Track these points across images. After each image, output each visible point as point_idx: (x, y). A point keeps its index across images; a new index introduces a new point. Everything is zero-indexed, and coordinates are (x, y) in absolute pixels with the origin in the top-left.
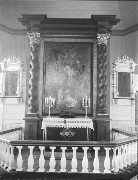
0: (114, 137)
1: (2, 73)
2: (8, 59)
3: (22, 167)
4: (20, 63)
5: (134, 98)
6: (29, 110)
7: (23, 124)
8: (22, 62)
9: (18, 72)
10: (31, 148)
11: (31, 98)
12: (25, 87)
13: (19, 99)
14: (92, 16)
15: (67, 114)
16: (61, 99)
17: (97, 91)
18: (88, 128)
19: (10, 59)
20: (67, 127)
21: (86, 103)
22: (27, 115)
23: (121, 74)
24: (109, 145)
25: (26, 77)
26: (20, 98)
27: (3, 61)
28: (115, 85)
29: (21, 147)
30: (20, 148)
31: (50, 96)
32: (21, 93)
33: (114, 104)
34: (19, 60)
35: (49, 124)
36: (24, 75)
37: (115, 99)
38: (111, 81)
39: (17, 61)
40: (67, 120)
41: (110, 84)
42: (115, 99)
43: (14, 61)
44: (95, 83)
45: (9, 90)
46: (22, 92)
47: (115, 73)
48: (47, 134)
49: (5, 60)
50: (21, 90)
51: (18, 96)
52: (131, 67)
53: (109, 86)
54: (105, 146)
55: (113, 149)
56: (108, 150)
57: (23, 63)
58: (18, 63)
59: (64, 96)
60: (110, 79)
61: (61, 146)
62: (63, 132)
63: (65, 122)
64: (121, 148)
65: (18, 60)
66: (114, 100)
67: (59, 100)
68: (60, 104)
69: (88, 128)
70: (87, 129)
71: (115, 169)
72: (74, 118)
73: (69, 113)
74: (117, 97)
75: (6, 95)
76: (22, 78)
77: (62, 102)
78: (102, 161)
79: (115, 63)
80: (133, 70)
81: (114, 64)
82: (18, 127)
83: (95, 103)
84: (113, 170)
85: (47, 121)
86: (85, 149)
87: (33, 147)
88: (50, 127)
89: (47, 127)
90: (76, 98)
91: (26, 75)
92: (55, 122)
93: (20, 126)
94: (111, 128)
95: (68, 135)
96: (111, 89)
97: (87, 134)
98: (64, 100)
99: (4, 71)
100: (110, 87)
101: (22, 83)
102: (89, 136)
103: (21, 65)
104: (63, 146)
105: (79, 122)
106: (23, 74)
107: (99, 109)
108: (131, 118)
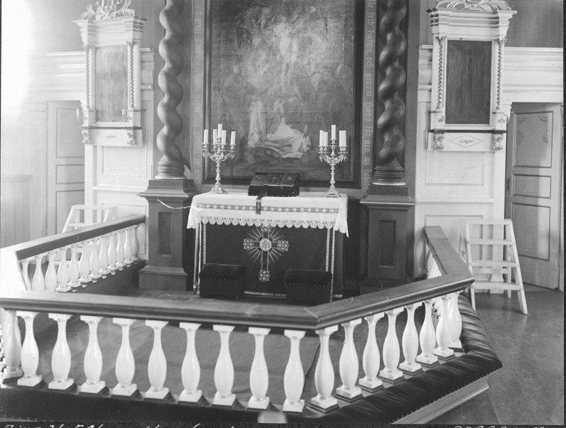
1: (84, 53)
2: (100, 10)
5: (503, 127)
6: (160, 169)
7: (142, 208)
8: (136, 17)
11: (165, 130)
13: (131, 132)
15: (270, 181)
16: (260, 133)
17: (375, 104)
18: (332, 230)
19: (104, 9)
20: (266, 225)
23: (457, 47)
25: (153, 64)
26: (135, 128)
27: (85, 14)
28: (435, 87)
29: (65, 318)
30: (62, 319)
31: (334, 127)
33: (430, 148)
34: (130, 11)
35: (247, 217)
36: (145, 57)
37: (432, 131)
38: (423, 73)
39: (122, 15)
40: (267, 201)
41: (420, 81)
42: (432, 131)
43: (115, 13)
44: (368, 78)
45: (106, 105)
46: (143, 111)
47: (436, 46)
48: (205, 243)
49: (90, 11)
50: (137, 105)
51: (131, 124)
52: (493, 23)
53: (415, 90)
54: (51, 309)
57: (139, 21)
58: (126, 20)
59: (270, 124)
62: (254, 239)
63: (259, 209)
65: (124, 10)
67: (252, 134)
68: (257, 149)
69: (332, 230)
70: (329, 234)
72: (296, 194)
73: (279, 176)
74: (442, 126)
75: (97, 119)
79: (435, 10)
80: (503, 31)
81: (433, 13)
82: (134, 215)
83: (366, 144)
85: (204, 206)
88: (212, 223)
89: (205, 222)
90: (305, 129)
92: (230, 207)
95: (268, 249)
96: (422, 97)
97: (328, 247)
98: (269, 136)
99: (89, 47)
100: (419, 92)
102: (333, 253)
105: (302, 210)
106: (142, 53)
107: (377, 167)
108: (491, 194)
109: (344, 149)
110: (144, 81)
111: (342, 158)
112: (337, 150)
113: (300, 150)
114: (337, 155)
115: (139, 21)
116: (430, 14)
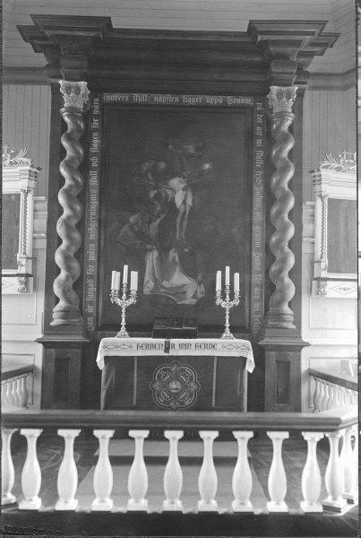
0: (312, 394)
3: (40, 495)
4: (28, 168)
7: (36, 357)
9: (22, 197)
10: (70, 435)
12: (42, 244)
14: (253, 28)
16: (155, 280)
21: (228, 292)
22: (47, 329)
23: (334, 204)
24: (315, 426)
26: (27, 276)
29: (37, 433)
30: (32, 435)
32: (31, 261)
33: (313, 293)
34: (25, 160)
37: (316, 279)
41: (304, 234)
42: (316, 279)
47: (319, 202)
50: (29, 253)
51: (22, 270)
55: (327, 435)
56: (313, 439)
57: (35, 170)
60: (303, 222)
61: (166, 429)
64: (339, 436)
65: (19, 158)
66: (314, 282)
71: (334, 499)
74: (324, 274)
76: (35, 217)
77: (156, 288)
78: (293, 474)
84: (329, 500)
86: (278, 439)
87: (76, 433)
91: (45, 205)
93: (28, 362)
94: (304, 367)
98: (165, 283)
101: (34, 232)
103: (30, 175)
104: (171, 429)
106: (35, 202)
109: (135, 293)
110: (36, 230)
111: (237, 302)
112: (128, 293)
113: (194, 296)
114: (128, 298)
115: (35, 170)
116: (313, 174)
